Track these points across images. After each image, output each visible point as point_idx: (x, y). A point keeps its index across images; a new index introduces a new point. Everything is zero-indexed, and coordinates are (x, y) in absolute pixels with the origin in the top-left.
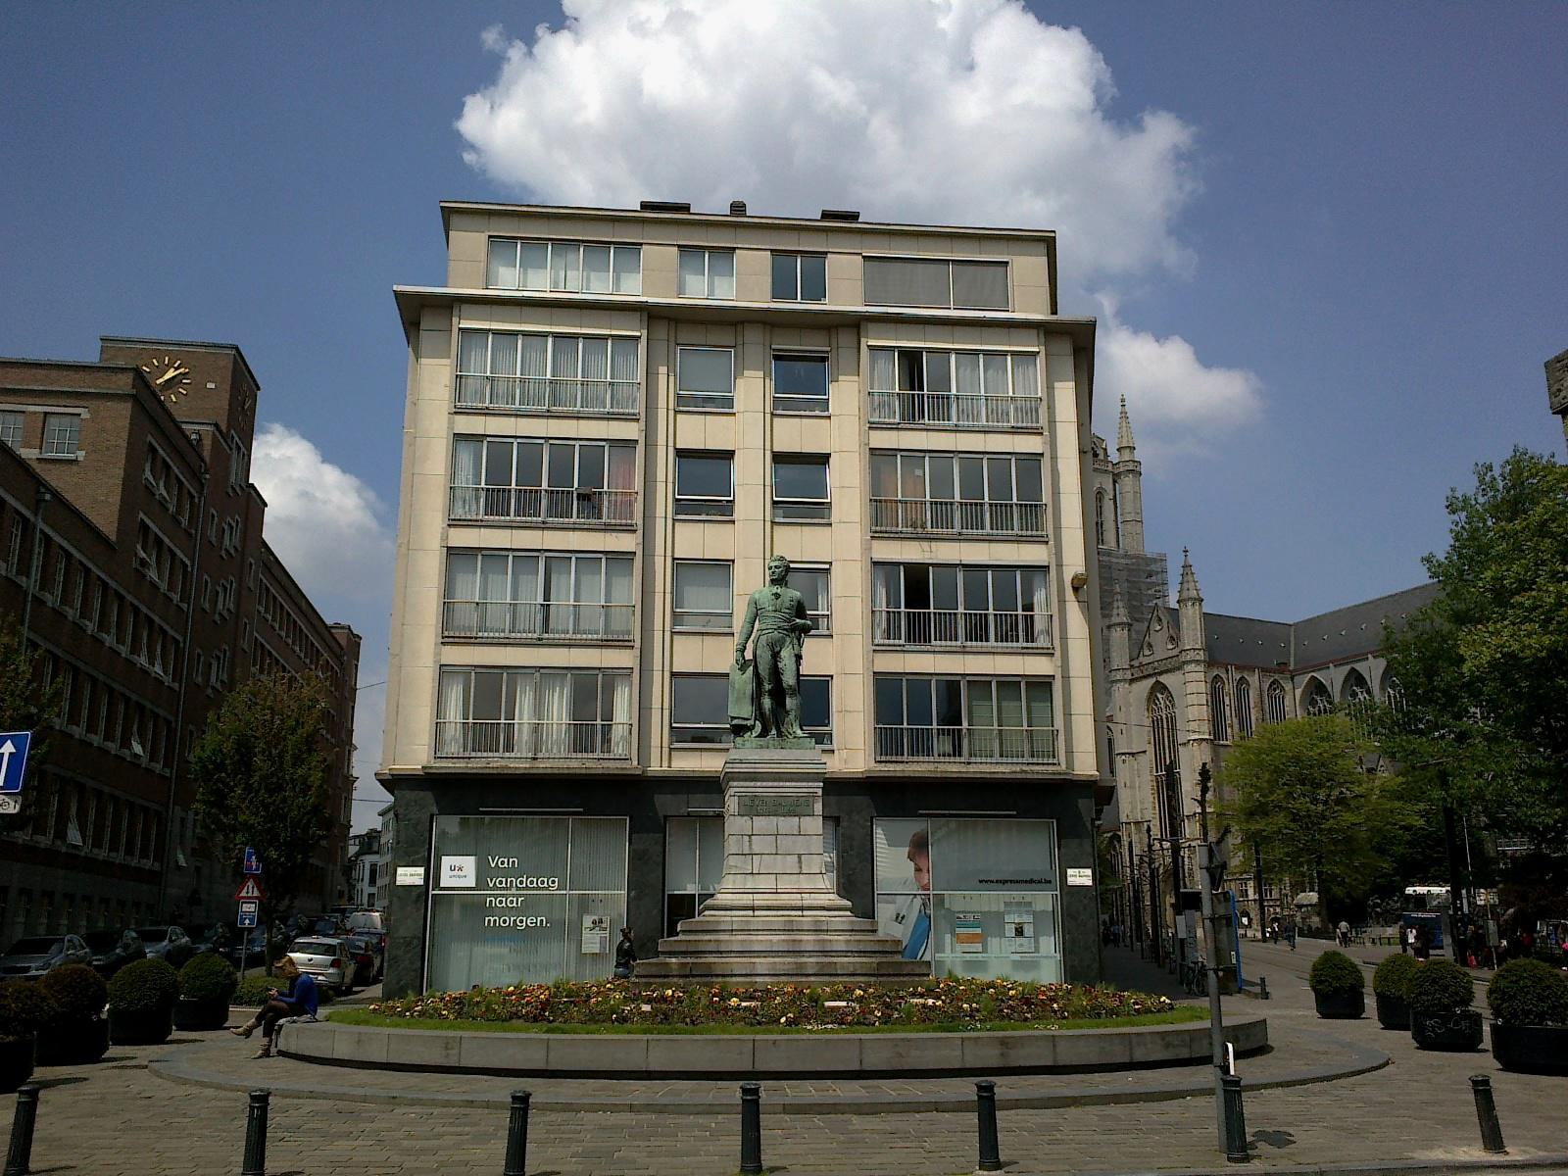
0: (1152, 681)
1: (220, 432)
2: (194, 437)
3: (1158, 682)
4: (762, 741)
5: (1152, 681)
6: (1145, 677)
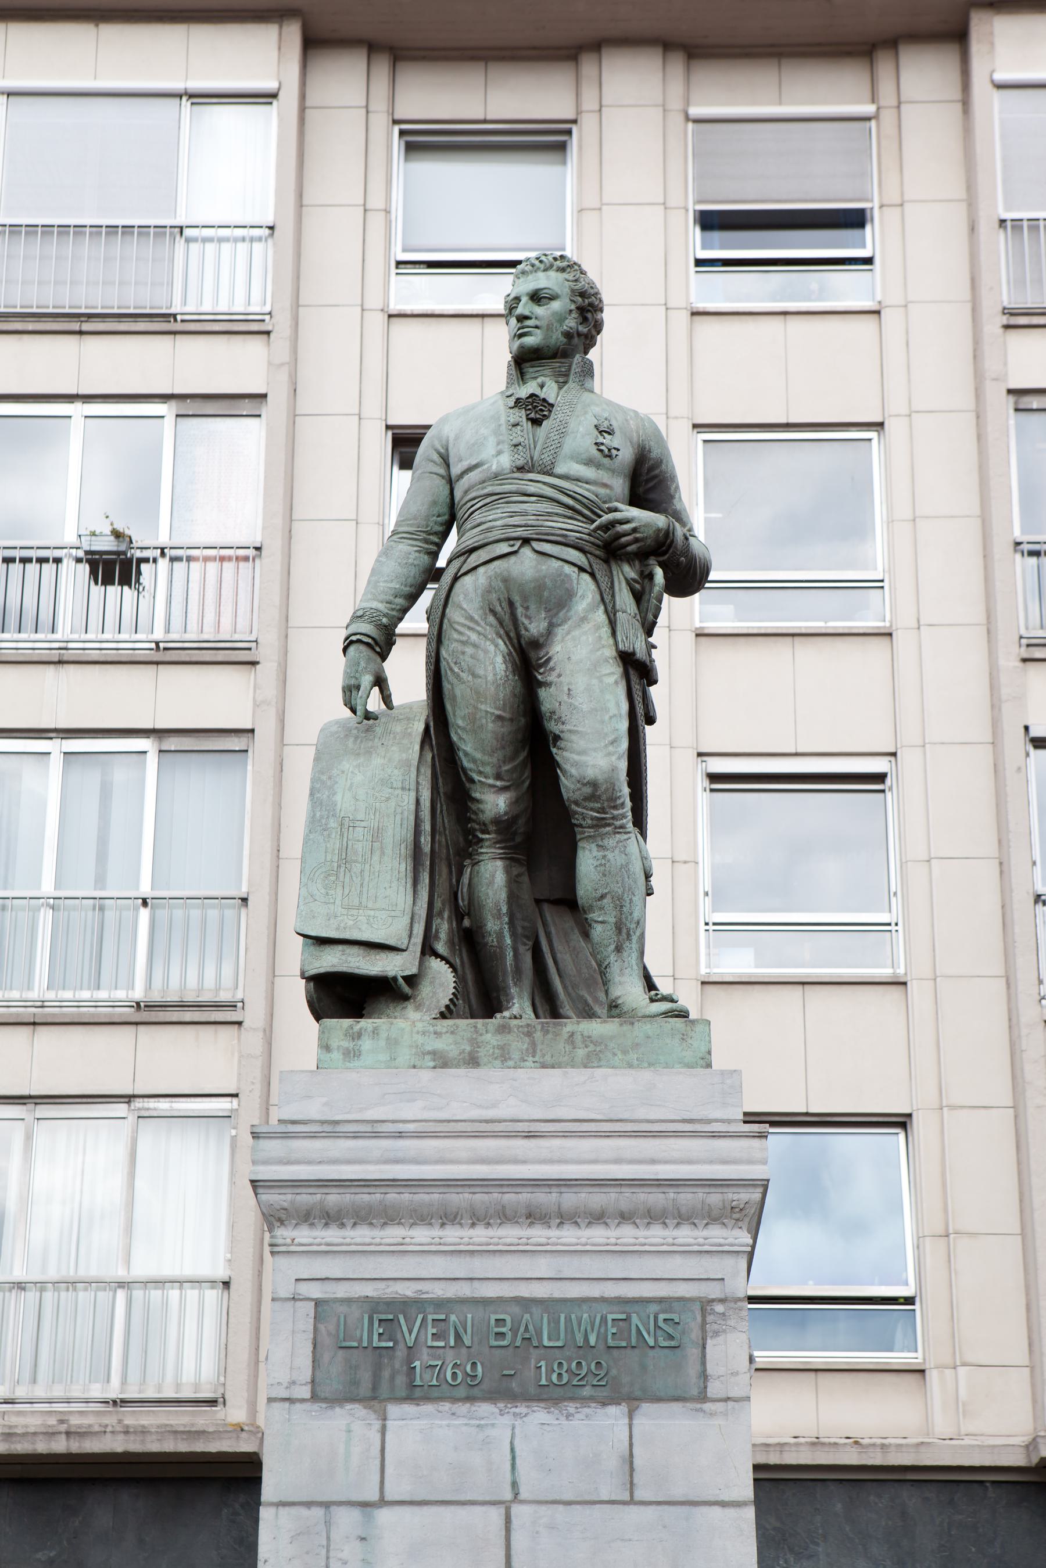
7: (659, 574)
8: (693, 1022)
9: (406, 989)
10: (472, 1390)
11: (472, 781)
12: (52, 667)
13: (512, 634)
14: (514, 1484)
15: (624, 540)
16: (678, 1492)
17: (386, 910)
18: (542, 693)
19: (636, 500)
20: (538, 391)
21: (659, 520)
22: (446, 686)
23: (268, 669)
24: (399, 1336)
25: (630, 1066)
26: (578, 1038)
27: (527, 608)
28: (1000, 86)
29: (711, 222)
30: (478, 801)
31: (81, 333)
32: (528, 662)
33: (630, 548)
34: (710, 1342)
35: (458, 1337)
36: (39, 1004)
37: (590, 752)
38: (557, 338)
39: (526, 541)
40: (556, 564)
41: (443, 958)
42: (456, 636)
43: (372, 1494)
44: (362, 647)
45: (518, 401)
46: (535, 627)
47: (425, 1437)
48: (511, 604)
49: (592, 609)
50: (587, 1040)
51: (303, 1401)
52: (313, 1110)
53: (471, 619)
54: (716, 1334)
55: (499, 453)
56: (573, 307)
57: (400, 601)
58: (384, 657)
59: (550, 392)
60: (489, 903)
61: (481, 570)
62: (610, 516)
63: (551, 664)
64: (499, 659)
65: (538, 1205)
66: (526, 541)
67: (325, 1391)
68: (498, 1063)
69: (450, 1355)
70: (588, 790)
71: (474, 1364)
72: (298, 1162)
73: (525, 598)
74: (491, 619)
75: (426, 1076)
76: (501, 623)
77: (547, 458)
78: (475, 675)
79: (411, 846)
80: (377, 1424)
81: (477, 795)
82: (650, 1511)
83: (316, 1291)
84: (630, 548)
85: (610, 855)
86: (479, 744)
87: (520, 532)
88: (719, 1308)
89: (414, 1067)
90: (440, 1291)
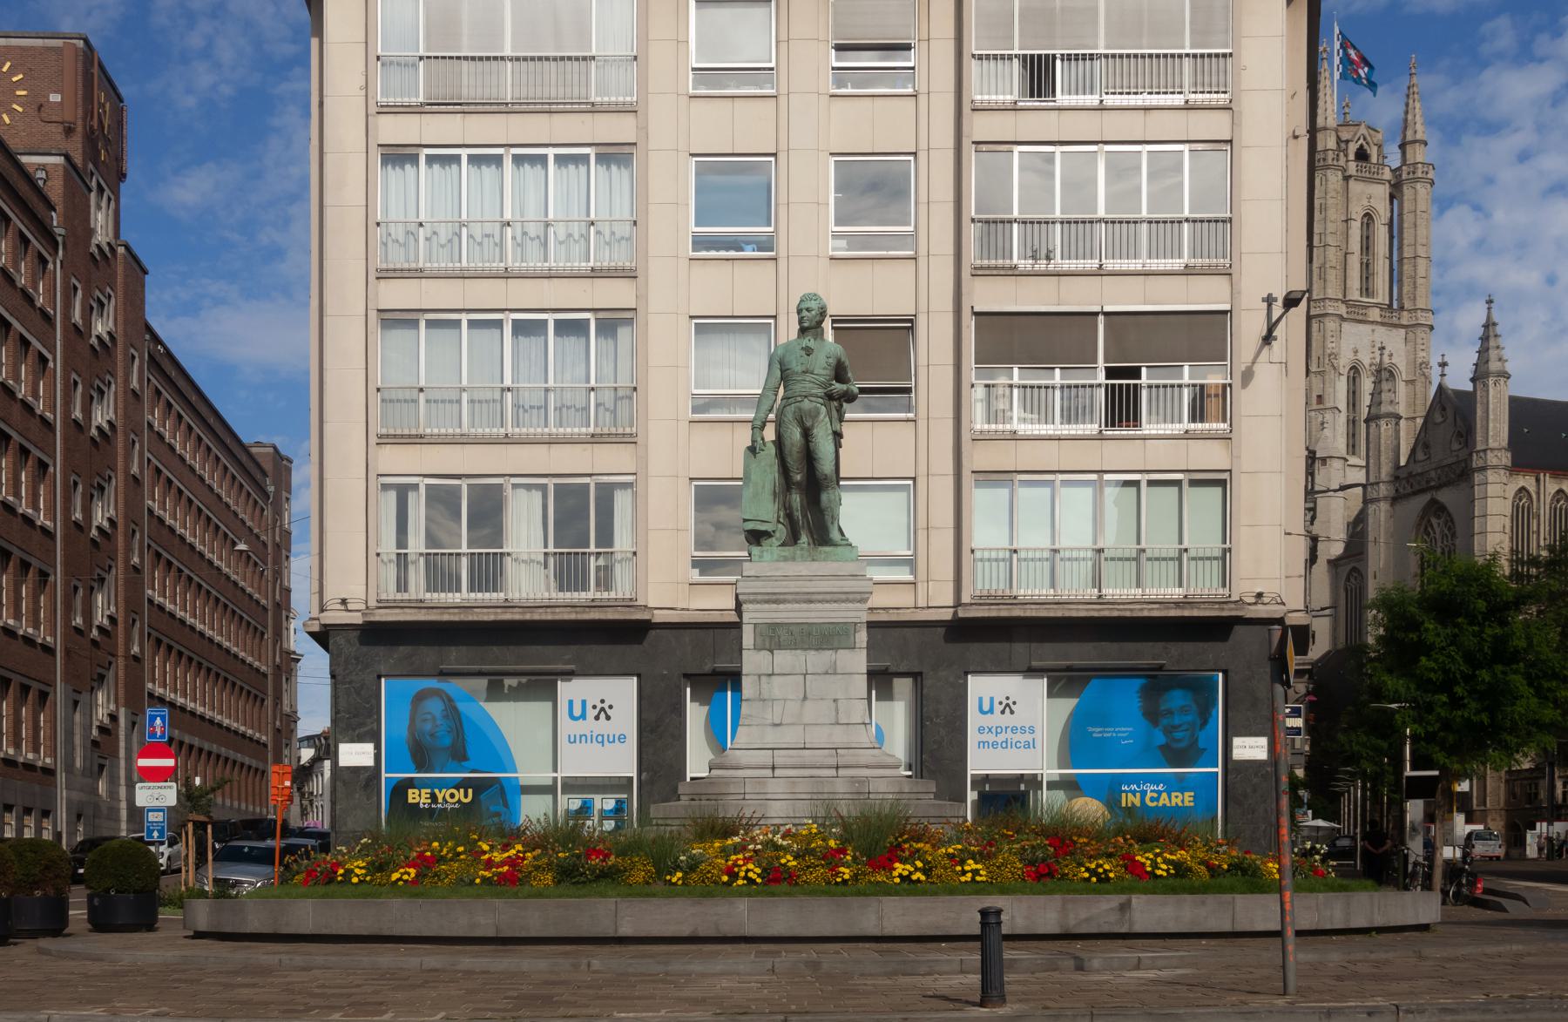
0: (1426, 498)
1: (74, 166)
2: (41, 174)
3: (1433, 501)
4: (787, 551)
5: (1426, 498)
6: (1415, 493)
29: (839, 48)
32: (807, 434)
36: (783, 37)
37: (826, 466)
46: (808, 424)
47: (784, 658)
75: (782, 564)
86: (794, 460)
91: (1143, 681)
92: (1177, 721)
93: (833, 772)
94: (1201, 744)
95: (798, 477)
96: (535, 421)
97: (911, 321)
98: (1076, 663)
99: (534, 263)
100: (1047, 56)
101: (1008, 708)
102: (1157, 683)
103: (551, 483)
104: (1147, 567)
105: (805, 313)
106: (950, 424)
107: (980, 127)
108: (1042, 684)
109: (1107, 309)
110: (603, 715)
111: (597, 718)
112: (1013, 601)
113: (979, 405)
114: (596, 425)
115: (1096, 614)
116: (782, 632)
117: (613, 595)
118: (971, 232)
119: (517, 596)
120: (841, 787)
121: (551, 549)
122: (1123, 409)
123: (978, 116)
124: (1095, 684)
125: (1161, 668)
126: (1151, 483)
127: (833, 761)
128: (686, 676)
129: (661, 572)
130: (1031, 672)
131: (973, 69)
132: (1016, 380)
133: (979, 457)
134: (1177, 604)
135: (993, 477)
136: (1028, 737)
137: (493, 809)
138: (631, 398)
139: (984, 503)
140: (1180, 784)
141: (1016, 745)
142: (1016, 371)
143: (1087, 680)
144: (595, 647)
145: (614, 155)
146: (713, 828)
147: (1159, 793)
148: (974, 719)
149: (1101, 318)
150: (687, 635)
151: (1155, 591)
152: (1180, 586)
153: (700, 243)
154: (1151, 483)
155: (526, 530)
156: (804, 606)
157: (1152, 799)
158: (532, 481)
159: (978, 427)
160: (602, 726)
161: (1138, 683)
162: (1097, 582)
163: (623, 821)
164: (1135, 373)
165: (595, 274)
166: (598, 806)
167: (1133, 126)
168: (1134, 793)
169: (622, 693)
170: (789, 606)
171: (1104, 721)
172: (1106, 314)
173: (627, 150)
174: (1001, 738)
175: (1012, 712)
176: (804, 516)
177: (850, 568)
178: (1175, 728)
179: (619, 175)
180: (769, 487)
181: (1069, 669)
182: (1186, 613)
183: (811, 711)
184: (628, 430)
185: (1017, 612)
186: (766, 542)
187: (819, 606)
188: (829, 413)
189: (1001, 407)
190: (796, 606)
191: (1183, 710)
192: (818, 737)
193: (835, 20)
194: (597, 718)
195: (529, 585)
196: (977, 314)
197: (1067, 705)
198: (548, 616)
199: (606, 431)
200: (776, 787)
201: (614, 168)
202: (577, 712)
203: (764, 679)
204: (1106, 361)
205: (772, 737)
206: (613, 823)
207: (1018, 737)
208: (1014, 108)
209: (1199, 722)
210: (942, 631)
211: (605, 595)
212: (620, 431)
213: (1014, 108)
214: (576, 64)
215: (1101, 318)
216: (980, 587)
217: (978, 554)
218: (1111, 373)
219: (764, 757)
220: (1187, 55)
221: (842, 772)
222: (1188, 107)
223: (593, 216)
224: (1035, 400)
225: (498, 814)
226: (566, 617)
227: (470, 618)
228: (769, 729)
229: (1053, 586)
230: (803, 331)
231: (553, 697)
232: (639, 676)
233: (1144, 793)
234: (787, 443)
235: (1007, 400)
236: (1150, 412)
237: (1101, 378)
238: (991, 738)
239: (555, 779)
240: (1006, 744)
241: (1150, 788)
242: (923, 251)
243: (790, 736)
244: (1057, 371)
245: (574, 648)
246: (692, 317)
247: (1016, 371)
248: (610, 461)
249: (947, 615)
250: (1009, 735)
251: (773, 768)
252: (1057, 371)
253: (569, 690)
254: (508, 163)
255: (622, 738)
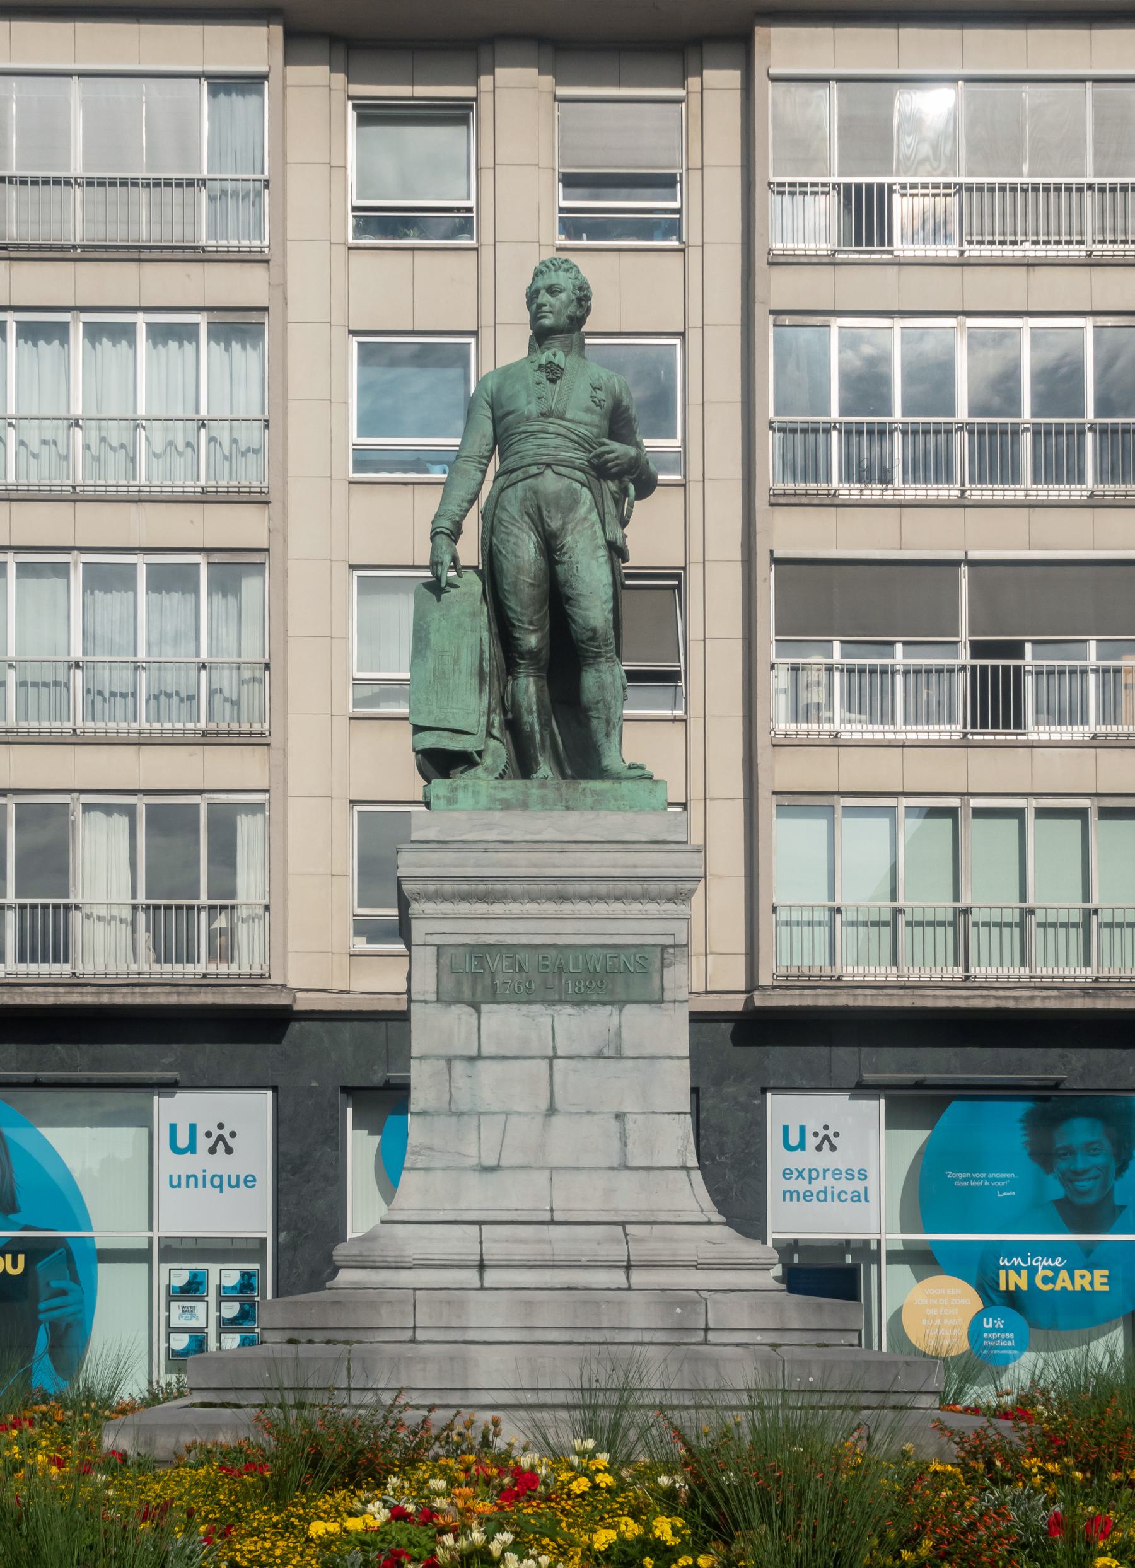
4: (514, 787)
7: (632, 488)
8: (656, 781)
9: (477, 758)
10: (525, 996)
11: (514, 626)
12: (134, 505)
13: (540, 529)
14: (554, 1048)
15: (610, 464)
16: (647, 1052)
17: (467, 711)
18: (559, 568)
19: (613, 435)
20: (552, 359)
21: (632, 451)
22: (497, 563)
23: (275, 506)
24: (486, 966)
25: (619, 809)
26: (587, 791)
27: (549, 512)
28: (775, 79)
29: (571, 181)
30: (518, 639)
31: (140, 260)
32: (550, 546)
33: (613, 470)
34: (665, 970)
35: (521, 967)
36: (487, 161)
38: (563, 320)
39: (549, 465)
40: (567, 481)
41: (498, 739)
42: (503, 529)
43: (474, 1052)
44: (444, 536)
45: (540, 366)
46: (555, 524)
47: (503, 1022)
48: (539, 509)
49: (590, 511)
50: (594, 792)
51: (431, 1002)
52: (432, 835)
53: (514, 518)
54: (669, 966)
55: (529, 403)
56: (574, 297)
57: (465, 505)
58: (456, 542)
59: (560, 358)
60: (525, 705)
61: (520, 484)
62: (603, 449)
63: (565, 550)
64: (532, 545)
65: (560, 891)
66: (549, 465)
67: (444, 997)
68: (539, 807)
69: (517, 977)
70: (590, 634)
71: (530, 982)
72: (424, 866)
73: (548, 505)
74: (527, 518)
75: (498, 815)
76: (533, 521)
77: (560, 407)
78: (516, 556)
79: (478, 668)
80: (476, 1016)
81: (517, 635)
82: (630, 1063)
83: (437, 940)
84: (613, 470)
85: (603, 676)
87: (544, 459)
88: (671, 950)
89: (490, 809)
90: (509, 940)
91: (1029, 1105)
92: (1080, 1165)
93: (618, 1278)
94: (1118, 1200)
95: (532, 641)
96: (119, 713)
97: (677, 577)
98: (931, 1077)
99: (114, 477)
100: (881, 187)
101: (827, 1142)
102: (1050, 1107)
103: (141, 803)
104: (1036, 936)
105: (544, 297)
106: (738, 724)
107: (779, 289)
108: (876, 1108)
109: (974, 555)
110: (221, 1147)
111: (212, 1150)
112: (836, 983)
113: (782, 698)
114: (210, 718)
115: (962, 1004)
116: (497, 964)
117: (234, 969)
118: (769, 444)
119: (89, 968)
120: (640, 1315)
121: (142, 899)
122: (996, 704)
123: (776, 271)
124: (956, 1108)
125: (1056, 1085)
126: (1041, 813)
127: (618, 1253)
128: (345, 1089)
129: (304, 940)
130: (861, 1089)
131: (772, 207)
132: (837, 658)
133: (781, 771)
134: (1085, 991)
135: (804, 802)
136: (858, 1185)
137: (55, 1284)
138: (261, 682)
139: (792, 842)
140: (1087, 1257)
141: (840, 1196)
142: (837, 645)
143: (948, 1100)
144: (208, 1047)
145: (238, 325)
146: (315, 1462)
147: (1057, 1270)
148: (776, 1157)
149: (964, 570)
150: (347, 1030)
151: (1045, 971)
152: (1087, 963)
153: (364, 460)
154: (1041, 813)
155: (105, 868)
156: (550, 907)
157: (1046, 1280)
158: (110, 801)
159: (781, 726)
160: (220, 1163)
161: (1020, 1108)
162: (961, 956)
163: (253, 1304)
164: (1015, 649)
165: (205, 498)
166: (213, 1282)
167: (1009, 288)
168: (1018, 1270)
169: (250, 1114)
170: (515, 907)
171: (972, 1164)
172: (972, 564)
173: (254, 317)
174: (817, 1186)
175: (229, 1150)
176: (545, 725)
177: (648, 826)
178: (1078, 1174)
179: (247, 360)
180: (468, 659)
181: (919, 1085)
182: (1100, 1004)
183: (567, 1139)
184: (257, 727)
185: (843, 1000)
186: (463, 779)
187: (582, 908)
188: (598, 504)
189: (814, 698)
190: (532, 907)
191: (1090, 1148)
192: (583, 1196)
193: (561, 141)
194: (212, 1150)
195: (109, 952)
196: (777, 561)
197: (914, 1139)
198: (135, 998)
199: (223, 727)
200: (488, 1314)
201: (236, 347)
202: (183, 1141)
203: (459, 1067)
204: (972, 632)
205: (478, 1197)
206: (236, 1306)
207: (843, 1185)
208: (831, 262)
209: (1113, 1167)
210: (727, 1028)
211: (223, 968)
212: (245, 727)
213: (831, 262)
214: (178, 191)
215: (964, 570)
216: (785, 962)
217: (783, 915)
218: (979, 650)
219: (460, 1242)
220: (1091, 187)
221: (639, 1278)
222: (1091, 263)
223: (203, 412)
224: (869, 691)
225: (63, 1293)
226: (163, 1000)
227: (18, 1000)
228: (473, 1179)
229: (895, 961)
230: (541, 336)
231: (144, 1119)
232: (275, 1089)
233: (1032, 1271)
234: (508, 566)
235: (823, 692)
236: (1037, 711)
237: (964, 657)
238: (802, 1185)
239: (151, 1240)
240: (823, 1196)
241: (1042, 1263)
242: (695, 473)
243: (519, 1194)
244: (899, 648)
245: (178, 1048)
246: (353, 567)
247: (837, 645)
248: (230, 770)
249: (736, 1004)
250: (830, 1181)
251: (482, 1267)
252: (899, 648)
253: (174, 1110)
254: (77, 334)
255: (250, 1181)
